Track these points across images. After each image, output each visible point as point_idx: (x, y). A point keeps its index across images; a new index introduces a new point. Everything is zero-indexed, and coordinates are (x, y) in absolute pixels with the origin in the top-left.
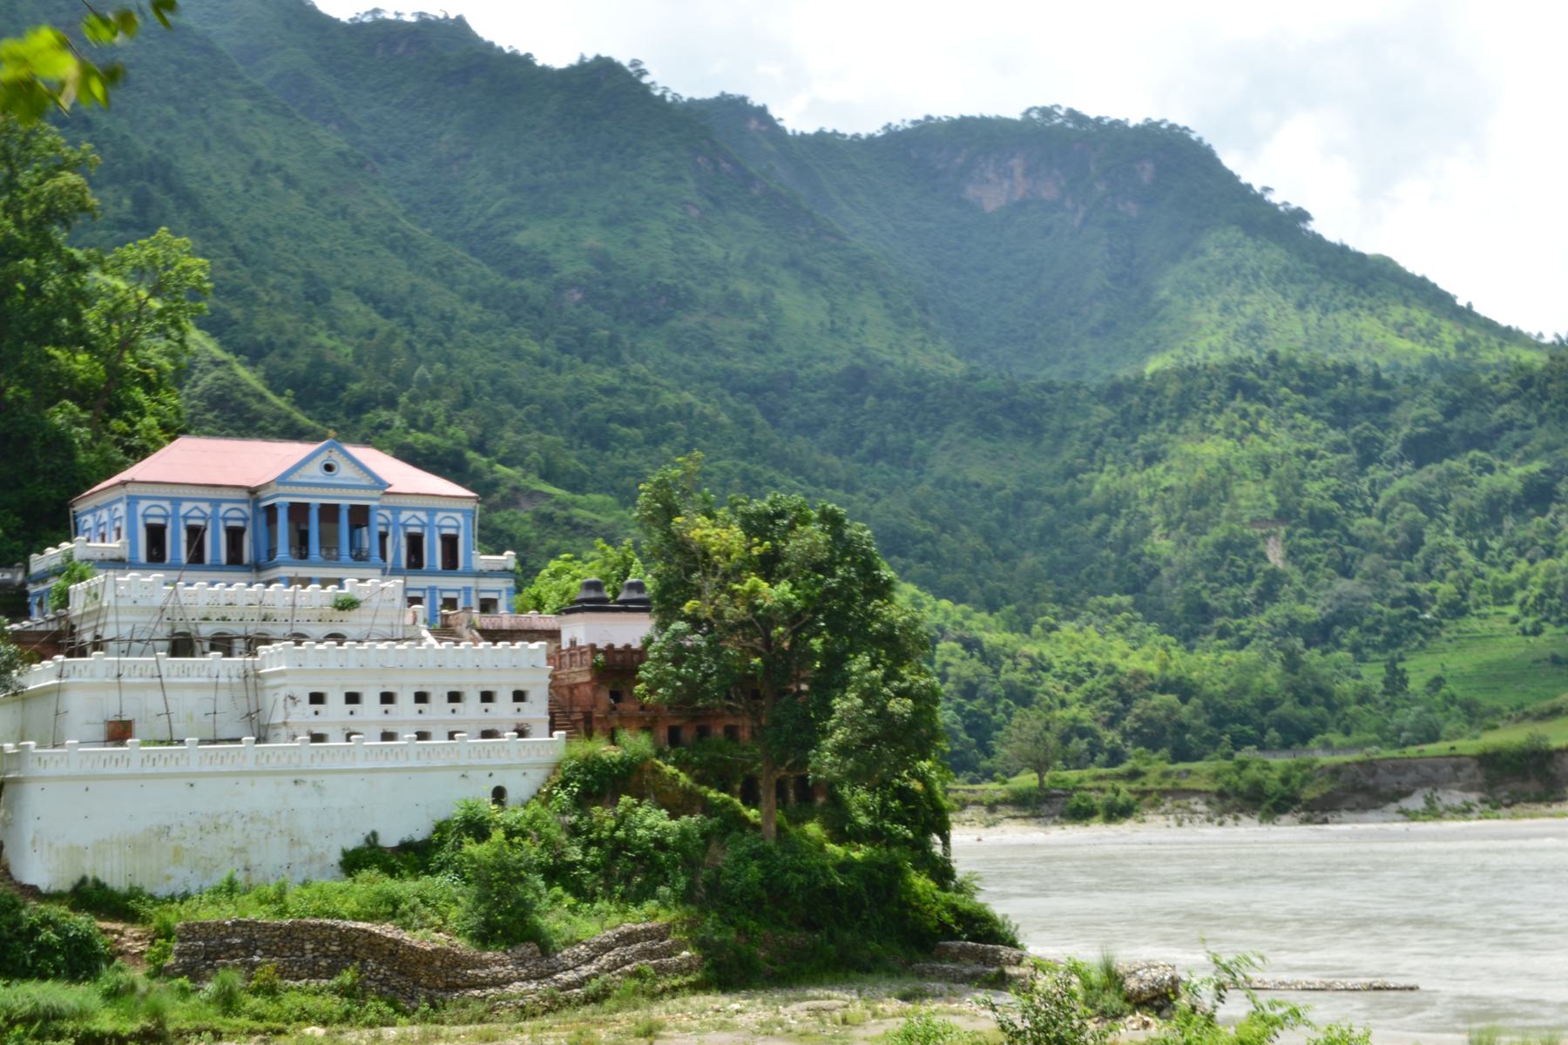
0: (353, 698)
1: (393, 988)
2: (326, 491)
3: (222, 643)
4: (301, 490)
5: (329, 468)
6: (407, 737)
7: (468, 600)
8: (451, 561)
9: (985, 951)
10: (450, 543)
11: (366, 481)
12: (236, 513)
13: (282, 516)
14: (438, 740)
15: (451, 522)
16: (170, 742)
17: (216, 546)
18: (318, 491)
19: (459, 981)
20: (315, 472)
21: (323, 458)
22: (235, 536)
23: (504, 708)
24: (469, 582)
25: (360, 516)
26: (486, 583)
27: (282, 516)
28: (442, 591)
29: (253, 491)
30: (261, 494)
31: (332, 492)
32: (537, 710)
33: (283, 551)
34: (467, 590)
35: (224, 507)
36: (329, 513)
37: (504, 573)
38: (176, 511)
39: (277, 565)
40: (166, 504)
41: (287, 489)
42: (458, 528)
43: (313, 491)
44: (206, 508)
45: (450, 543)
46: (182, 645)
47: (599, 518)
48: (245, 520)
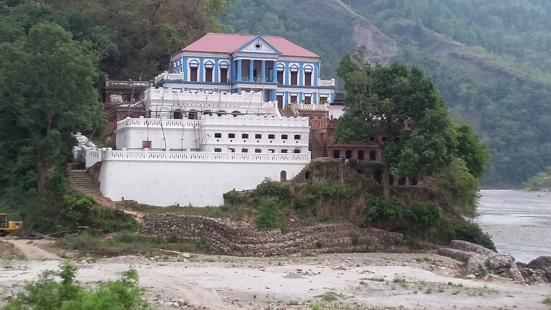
0: (232, 136)
1: (222, 242)
2: (256, 55)
3: (193, 115)
4: (246, 55)
5: (258, 46)
6: (252, 150)
7: (301, 97)
8: (308, 82)
9: (465, 245)
10: (308, 75)
11: (272, 52)
12: (224, 63)
13: (240, 64)
14: (290, 154)
15: (308, 67)
16: (182, 150)
17: (216, 76)
18: (253, 55)
19: (246, 241)
20: (252, 48)
21: (255, 43)
22: (224, 71)
23: (291, 142)
24: (316, 91)
25: (270, 65)
26: (322, 91)
27: (240, 64)
28: (304, 94)
29: (231, 55)
30: (234, 56)
31: (258, 56)
32: (304, 142)
33: (239, 79)
34: (315, 94)
35: (220, 60)
36: (258, 63)
37: (331, 88)
38: (202, 62)
39: (237, 83)
40: (284, 63)
41: (241, 55)
42: (312, 69)
43: (251, 55)
44: (213, 61)
45: (308, 75)
46: (177, 115)
47: (476, 55)
48: (228, 65)
